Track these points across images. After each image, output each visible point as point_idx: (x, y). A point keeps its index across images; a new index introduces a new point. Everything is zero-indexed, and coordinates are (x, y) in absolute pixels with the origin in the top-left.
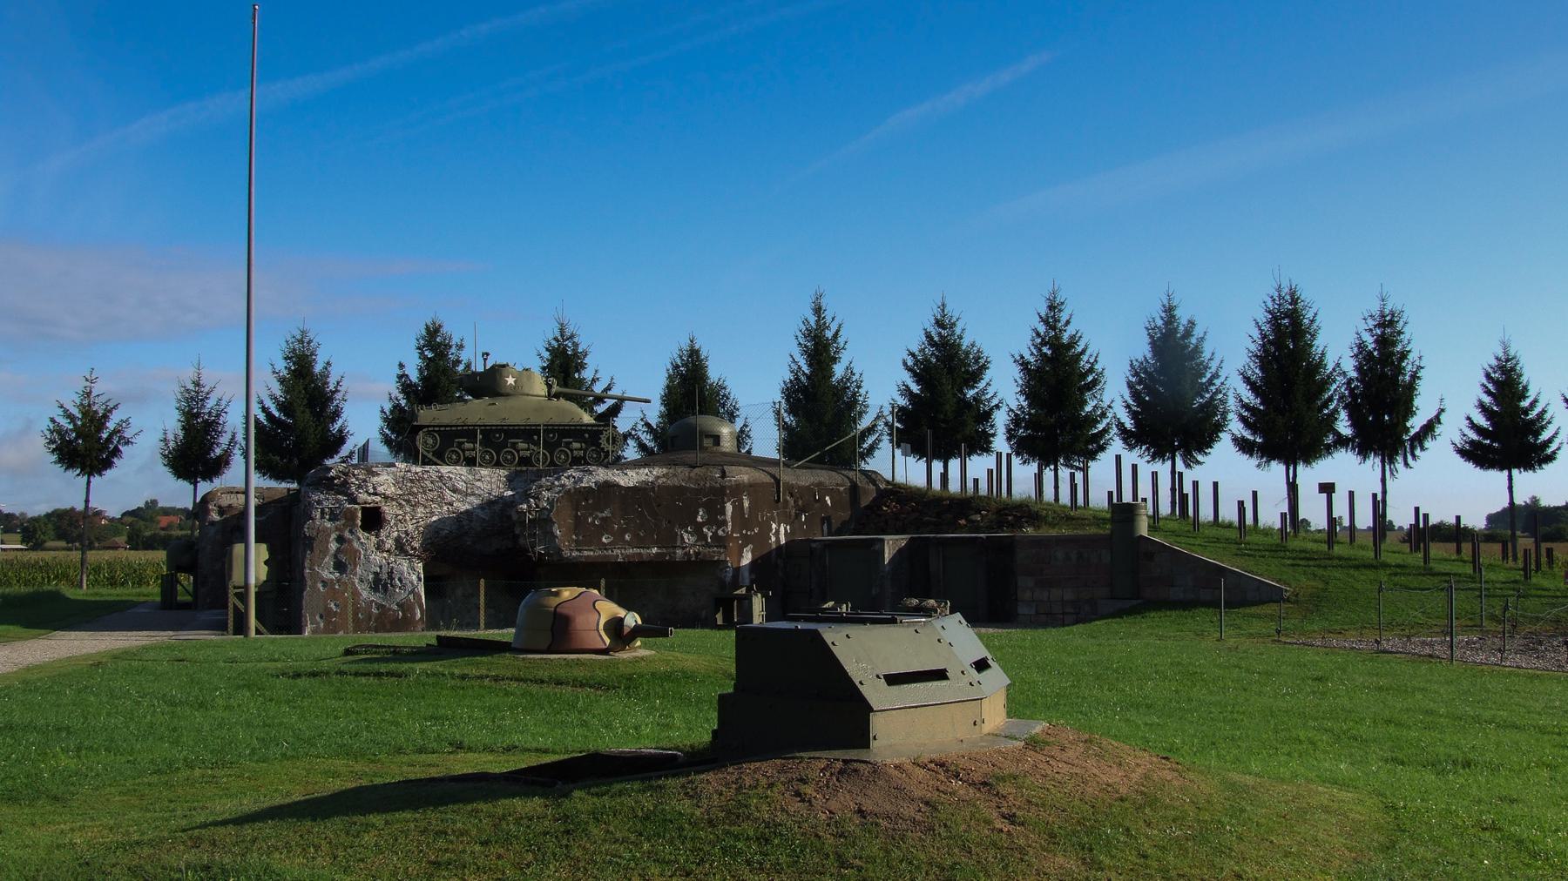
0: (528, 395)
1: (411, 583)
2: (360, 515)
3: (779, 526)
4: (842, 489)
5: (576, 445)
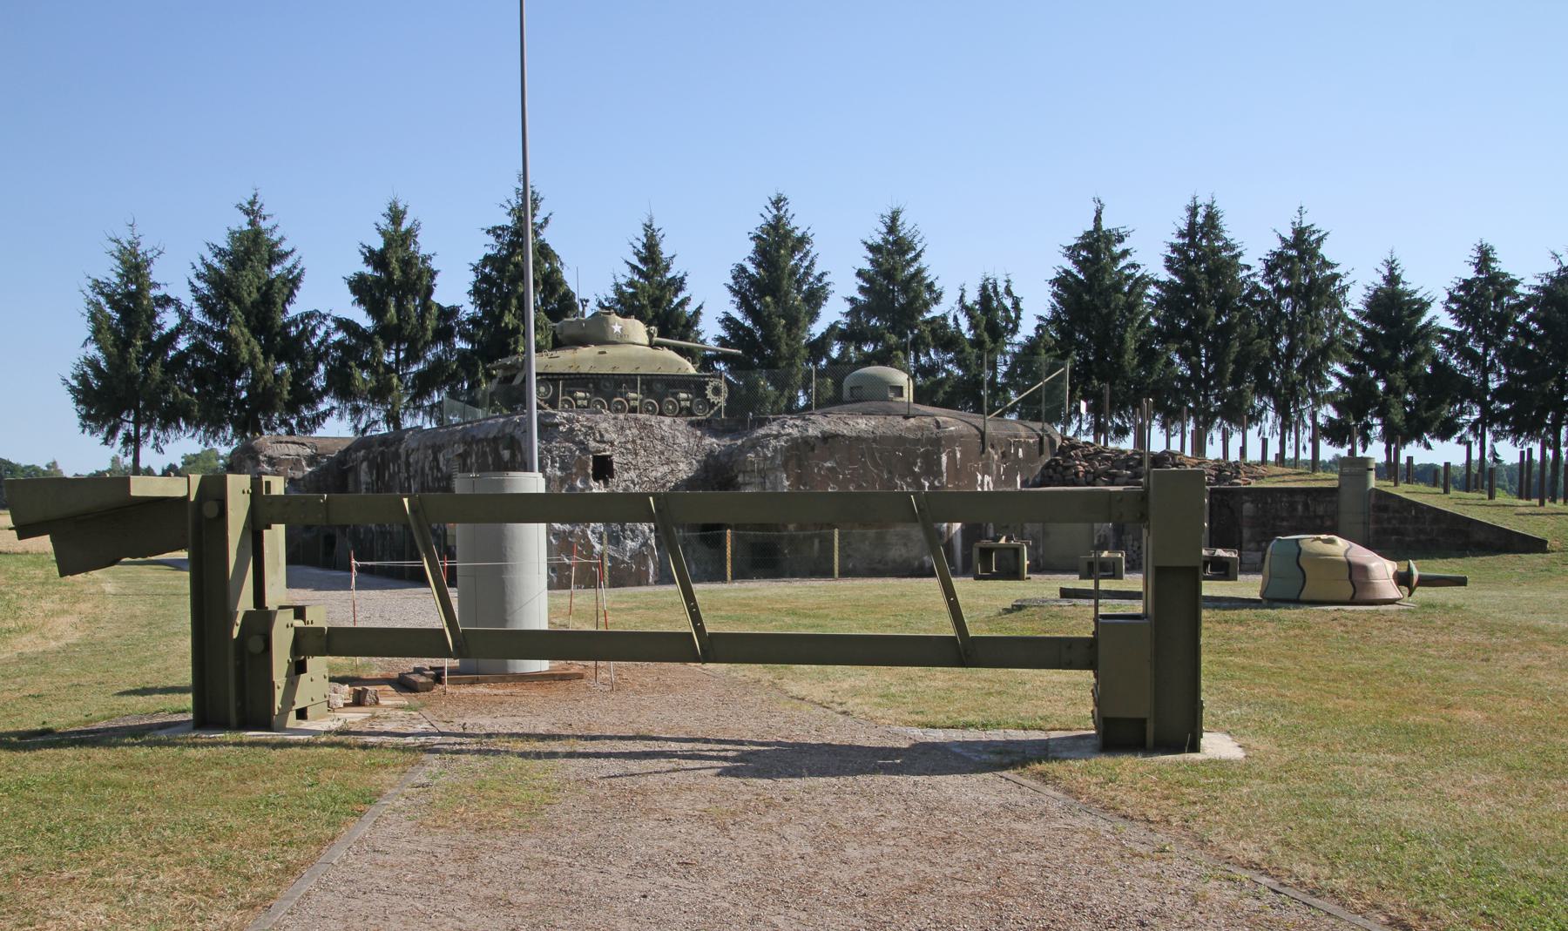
0: (634, 344)
1: (643, 533)
2: (591, 464)
3: (983, 477)
4: (1031, 441)
5: (683, 395)
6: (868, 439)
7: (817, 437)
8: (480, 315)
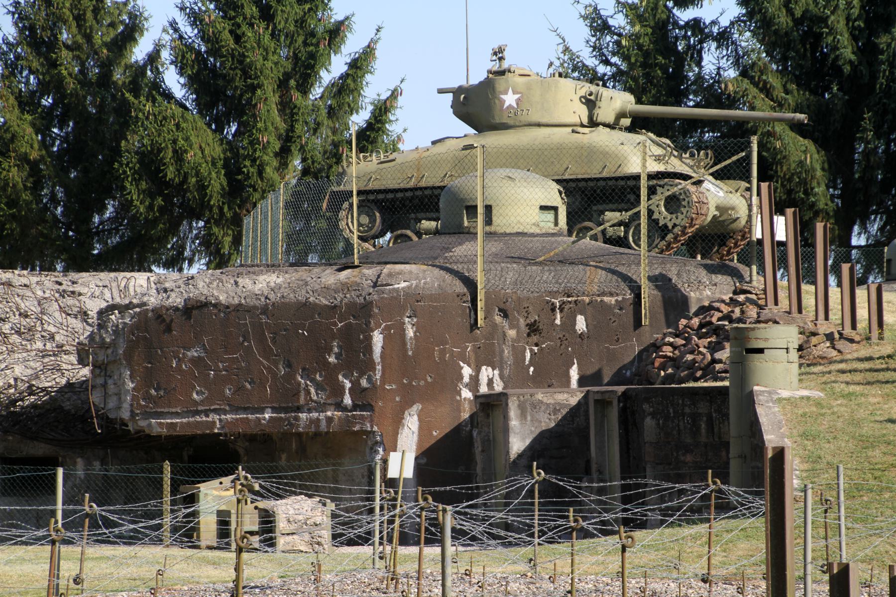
0: (539, 125)
3: (478, 371)
6: (255, 307)
7: (176, 309)
8: (208, 99)
